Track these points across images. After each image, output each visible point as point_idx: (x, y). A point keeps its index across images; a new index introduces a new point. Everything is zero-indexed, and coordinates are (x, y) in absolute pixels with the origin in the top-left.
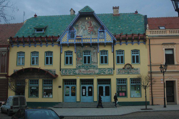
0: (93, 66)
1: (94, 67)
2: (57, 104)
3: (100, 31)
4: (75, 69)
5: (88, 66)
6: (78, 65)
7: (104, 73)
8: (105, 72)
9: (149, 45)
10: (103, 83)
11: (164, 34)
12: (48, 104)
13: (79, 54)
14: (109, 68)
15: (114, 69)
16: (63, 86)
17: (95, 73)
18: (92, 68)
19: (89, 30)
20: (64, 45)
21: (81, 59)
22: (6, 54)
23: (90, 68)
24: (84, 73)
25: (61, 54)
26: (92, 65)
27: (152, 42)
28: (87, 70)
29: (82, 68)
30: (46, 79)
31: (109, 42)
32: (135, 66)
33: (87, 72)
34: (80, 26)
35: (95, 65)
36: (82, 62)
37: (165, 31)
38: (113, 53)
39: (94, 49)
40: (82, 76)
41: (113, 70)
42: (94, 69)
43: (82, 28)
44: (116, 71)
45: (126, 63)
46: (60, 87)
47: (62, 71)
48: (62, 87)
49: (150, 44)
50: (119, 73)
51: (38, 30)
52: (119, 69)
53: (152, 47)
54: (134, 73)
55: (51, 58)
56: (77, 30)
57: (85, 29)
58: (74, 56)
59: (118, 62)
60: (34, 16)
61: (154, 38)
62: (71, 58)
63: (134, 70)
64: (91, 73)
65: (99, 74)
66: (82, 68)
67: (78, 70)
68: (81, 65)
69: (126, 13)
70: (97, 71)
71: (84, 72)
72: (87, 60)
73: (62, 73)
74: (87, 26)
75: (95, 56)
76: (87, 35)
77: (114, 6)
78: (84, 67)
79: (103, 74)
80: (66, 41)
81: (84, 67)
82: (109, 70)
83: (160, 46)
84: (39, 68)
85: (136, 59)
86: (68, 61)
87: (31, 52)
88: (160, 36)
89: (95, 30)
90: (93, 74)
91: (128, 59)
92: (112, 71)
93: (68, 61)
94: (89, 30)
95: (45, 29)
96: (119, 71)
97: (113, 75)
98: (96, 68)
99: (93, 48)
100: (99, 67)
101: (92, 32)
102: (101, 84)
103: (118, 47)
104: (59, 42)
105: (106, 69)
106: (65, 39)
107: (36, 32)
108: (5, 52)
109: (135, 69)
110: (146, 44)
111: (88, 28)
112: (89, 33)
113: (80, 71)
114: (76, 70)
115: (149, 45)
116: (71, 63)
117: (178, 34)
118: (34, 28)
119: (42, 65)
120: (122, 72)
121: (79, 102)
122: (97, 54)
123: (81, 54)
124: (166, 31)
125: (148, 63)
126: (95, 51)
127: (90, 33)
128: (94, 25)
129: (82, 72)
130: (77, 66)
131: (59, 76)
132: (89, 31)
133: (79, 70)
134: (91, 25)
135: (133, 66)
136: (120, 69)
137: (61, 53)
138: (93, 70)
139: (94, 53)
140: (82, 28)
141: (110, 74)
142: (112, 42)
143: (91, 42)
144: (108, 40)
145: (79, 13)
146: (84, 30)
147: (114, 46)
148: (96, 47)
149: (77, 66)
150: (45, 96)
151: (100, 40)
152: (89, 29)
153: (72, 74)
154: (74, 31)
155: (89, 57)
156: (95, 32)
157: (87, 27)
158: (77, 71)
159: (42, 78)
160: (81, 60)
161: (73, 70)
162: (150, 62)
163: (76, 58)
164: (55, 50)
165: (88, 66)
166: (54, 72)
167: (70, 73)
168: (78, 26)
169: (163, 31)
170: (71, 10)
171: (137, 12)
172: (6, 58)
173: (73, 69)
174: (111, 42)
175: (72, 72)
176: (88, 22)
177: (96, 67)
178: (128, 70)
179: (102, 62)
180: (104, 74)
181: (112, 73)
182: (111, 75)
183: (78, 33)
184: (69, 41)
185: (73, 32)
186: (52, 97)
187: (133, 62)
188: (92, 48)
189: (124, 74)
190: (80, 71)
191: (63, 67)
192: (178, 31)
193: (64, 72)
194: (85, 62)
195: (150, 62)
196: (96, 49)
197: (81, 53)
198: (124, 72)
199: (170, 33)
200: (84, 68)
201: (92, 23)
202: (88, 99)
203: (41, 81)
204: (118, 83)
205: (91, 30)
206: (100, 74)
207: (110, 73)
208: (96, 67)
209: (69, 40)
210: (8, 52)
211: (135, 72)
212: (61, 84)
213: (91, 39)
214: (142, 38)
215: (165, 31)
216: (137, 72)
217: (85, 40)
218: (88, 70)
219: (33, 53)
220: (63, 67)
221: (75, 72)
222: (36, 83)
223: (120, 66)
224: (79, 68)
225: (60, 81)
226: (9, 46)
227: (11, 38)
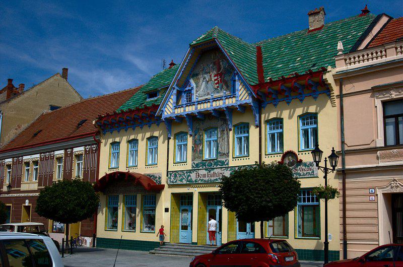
0: (220, 162)
4: (190, 171)
5: (211, 162)
12: (120, 243)
23: (215, 167)
24: (204, 179)
28: (210, 172)
29: (201, 168)
31: (245, 102)
45: (286, 149)
54: (304, 175)
63: (304, 168)
64: (216, 178)
66: (201, 168)
67: (195, 172)
71: (204, 176)
78: (205, 166)
81: (205, 166)
98: (226, 166)
109: (305, 165)
112: (216, 89)
113: (197, 174)
117: (393, 56)
122: (227, 133)
127: (218, 87)
128: (224, 68)
132: (216, 84)
143: (184, 114)
146: (207, 82)
149: (194, 163)
151: (199, 107)
152: (216, 78)
153: (185, 183)
158: (193, 176)
160: (200, 150)
161: (187, 173)
165: (211, 162)
167: (181, 180)
172: (96, 155)
174: (248, 102)
175: (185, 177)
176: (214, 64)
184: (176, 113)
186: (297, 237)
190: (197, 174)
201: (221, 63)
203: (139, 197)
209: (176, 110)
211: (305, 172)
213: (184, 106)
216: (311, 172)
218: (212, 172)
222: (313, 198)
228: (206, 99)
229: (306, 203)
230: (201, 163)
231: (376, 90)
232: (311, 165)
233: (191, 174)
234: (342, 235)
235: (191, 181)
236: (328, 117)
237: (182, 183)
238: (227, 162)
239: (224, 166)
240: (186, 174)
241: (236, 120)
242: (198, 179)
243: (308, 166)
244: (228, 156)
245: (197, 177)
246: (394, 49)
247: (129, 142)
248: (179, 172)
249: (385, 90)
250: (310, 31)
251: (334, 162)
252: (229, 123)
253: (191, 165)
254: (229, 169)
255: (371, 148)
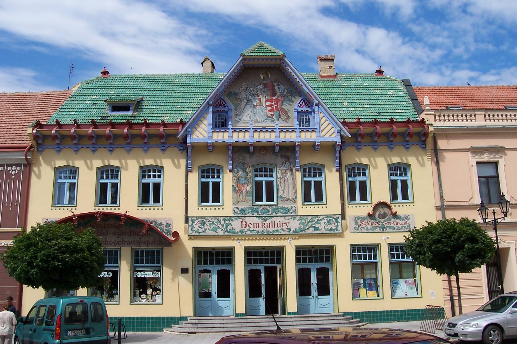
0: (282, 208)
1: (285, 213)
2: (175, 323)
4: (230, 218)
5: (268, 207)
7: (316, 229)
8: (317, 226)
10: (204, 260)
12: (141, 322)
14: (330, 216)
15: (343, 217)
16: (194, 267)
18: (280, 214)
19: (270, 108)
22: (20, 171)
23: (274, 214)
26: (280, 205)
28: (265, 220)
30: (143, 248)
32: (399, 208)
33: (266, 226)
34: (243, 95)
35: (288, 205)
39: (283, 161)
45: (375, 201)
47: (192, 224)
48: (190, 271)
50: (356, 229)
51: (116, 108)
52: (356, 219)
54: (398, 228)
55: (157, 187)
58: (227, 181)
59: (353, 198)
64: (276, 228)
65: (299, 234)
66: (250, 215)
67: (240, 220)
70: (295, 224)
71: (256, 225)
72: (263, 193)
78: (257, 212)
80: (206, 135)
81: (257, 212)
82: (329, 222)
84: (124, 215)
85: (400, 189)
86: (210, 194)
90: (282, 232)
91: (379, 188)
92: (337, 222)
93: (210, 194)
94: (270, 108)
95: (138, 105)
96: (356, 222)
97: (340, 235)
98: (293, 214)
99: (282, 156)
101: (276, 114)
105: (321, 217)
106: (203, 133)
108: (17, 165)
110: (427, 148)
112: (269, 117)
113: (244, 223)
114: (232, 219)
116: (217, 199)
119: (128, 204)
120: (364, 226)
122: (292, 175)
125: (434, 201)
127: (272, 115)
129: (250, 225)
130: (236, 210)
131: (184, 237)
132: (269, 111)
133: (242, 222)
135: (395, 208)
136: (360, 217)
138: (282, 220)
141: (332, 232)
142: (338, 139)
147: (342, 151)
148: (289, 154)
149: (237, 208)
150: (138, 299)
152: (269, 103)
154: (226, 109)
155: (270, 185)
158: (236, 225)
159: (130, 243)
161: (224, 220)
162: (442, 197)
163: (233, 186)
166: (168, 225)
167: (215, 230)
168: (236, 94)
170: (204, 62)
172: (19, 183)
173: (225, 218)
174: (335, 140)
175: (220, 226)
176: (265, 86)
177: (291, 211)
178: (382, 220)
179: (307, 198)
180: (316, 232)
181: (339, 228)
187: (394, 197)
188: (279, 158)
189: (372, 231)
190: (244, 223)
191: (195, 210)
192: (515, 115)
193: (196, 227)
194: (258, 198)
195: (442, 197)
198: (370, 227)
199: (486, 120)
200: (256, 214)
201: (276, 88)
203: (126, 253)
205: (274, 106)
206: (303, 232)
207: (331, 229)
208: (291, 211)
211: (400, 226)
212: (189, 264)
214: (415, 136)
217: (262, 134)
218: (269, 221)
221: (229, 227)
223: (358, 210)
226: (31, 147)
228: (264, 128)
229: (367, 260)
230: (249, 208)
231: (475, 151)
232: (406, 219)
233: (231, 222)
234: (448, 292)
235: (232, 231)
236: (421, 172)
237: (216, 234)
238: (293, 209)
239: (289, 214)
240: (222, 222)
241: (309, 160)
242: (246, 229)
243: (403, 220)
244: (295, 202)
245: (244, 226)
246: (433, 116)
247: (58, 170)
248: (210, 219)
249: (480, 152)
250: (322, 77)
251: (484, 214)
252: (297, 161)
253: (232, 212)
254: (297, 218)
255: (469, 206)
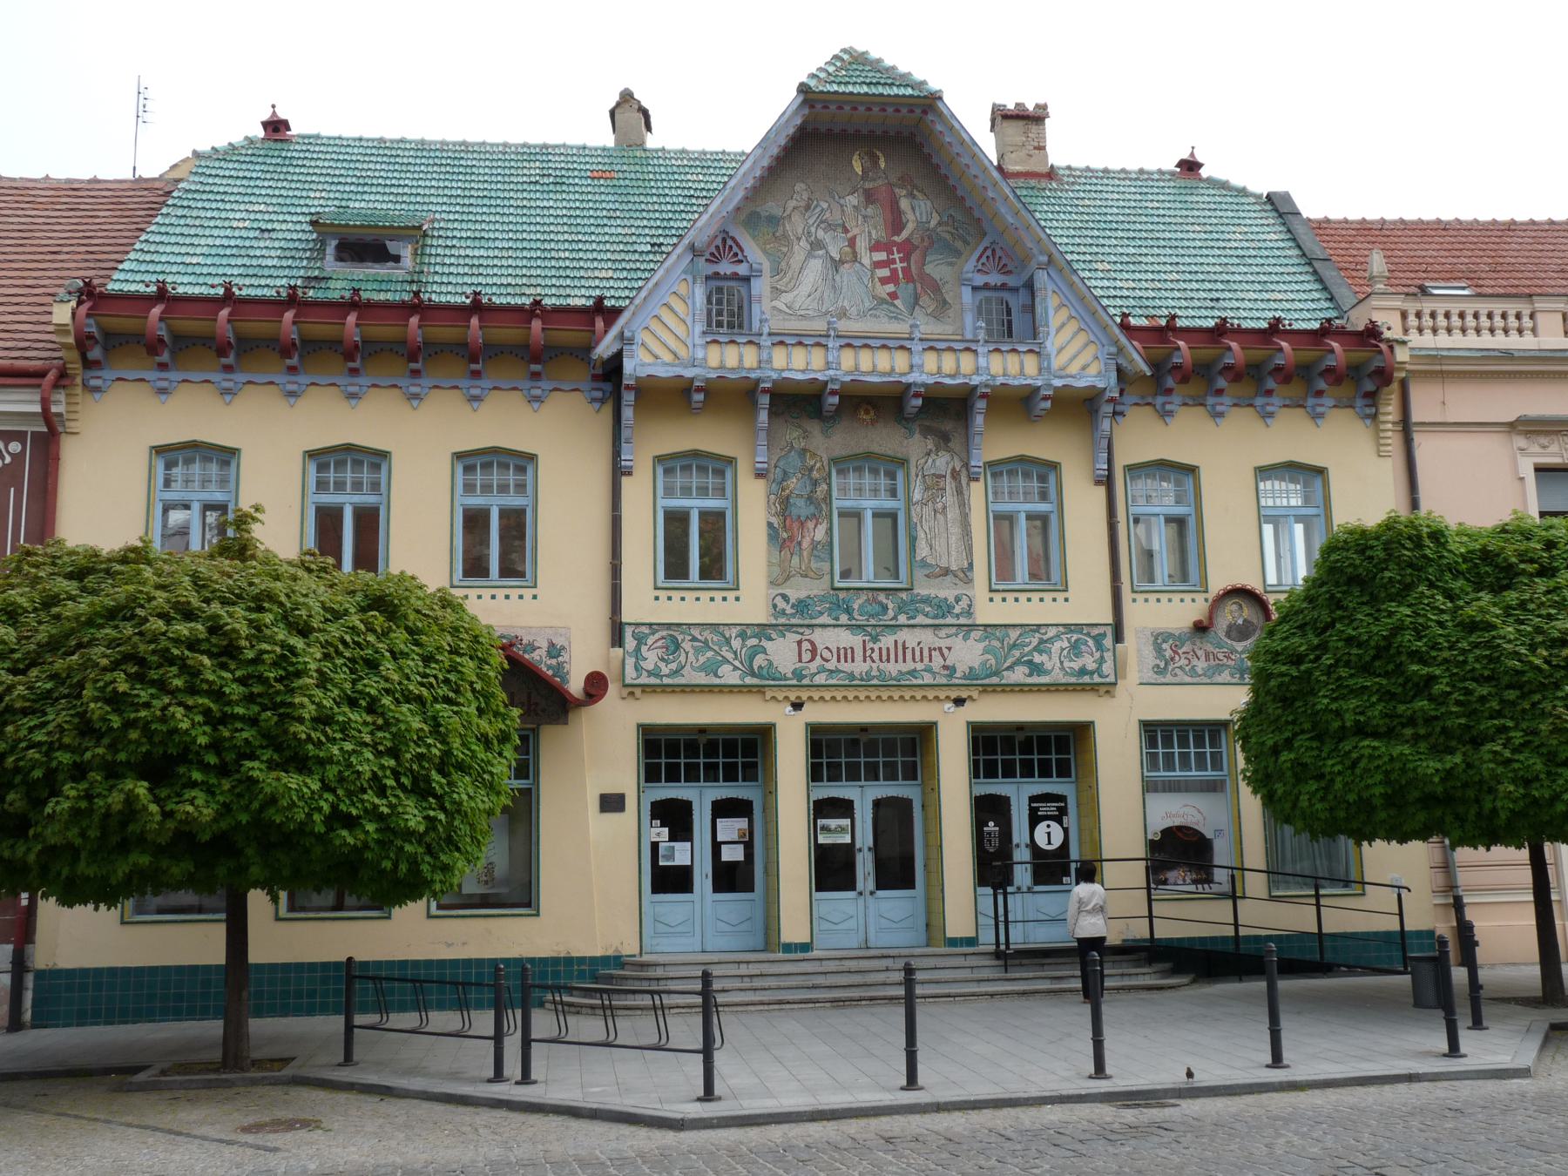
0: (927, 600)
1: (936, 617)
3: (980, 280)
4: (762, 630)
5: (882, 597)
6: (794, 595)
7: (1036, 669)
8: (1037, 659)
9: (1406, 426)
11: (1528, 336)
13: (793, 483)
14: (1078, 627)
15: (1118, 637)
17: (951, 670)
19: (885, 272)
20: (676, 397)
21: (820, 534)
23: (902, 619)
24: (843, 666)
25: (625, 480)
27: (1424, 404)
28: (875, 639)
33: (876, 656)
34: (796, 225)
36: (826, 566)
37: (1526, 312)
38: (1102, 490)
40: (931, 694)
41: (1108, 642)
42: (943, 633)
43: (817, 245)
44: (1136, 651)
45: (1217, 584)
46: (612, 803)
49: (1416, 416)
53: (1425, 447)
56: (766, 266)
57: (842, 262)
60: (260, 133)
61: (1442, 369)
62: (715, 524)
64: (910, 665)
65: (987, 684)
67: (792, 637)
68: (816, 588)
69: (1106, 171)
70: (968, 654)
71: (846, 654)
73: (637, 668)
74: (867, 230)
75: (945, 508)
76: (862, 315)
77: (999, 102)
78: (849, 611)
79: (1030, 680)
81: (849, 611)
82: (1075, 649)
83: (1493, 447)
86: (695, 551)
87: (311, 454)
88: (1488, 356)
89: (937, 269)
90: (928, 679)
93: (695, 551)
94: (885, 272)
96: (1159, 651)
97: (1104, 689)
98: (962, 621)
99: (926, 431)
100: (989, 611)
102: (673, 777)
103: (1140, 438)
104: (612, 369)
105: (1052, 632)
107: (330, 264)
108: (19, 436)
110: (1382, 418)
111: (876, 247)
113: (806, 645)
114: (759, 631)
115: (1406, 426)
116: (714, 567)
118: (313, 223)
120: (1183, 662)
121: (806, 947)
122: (959, 492)
123: (815, 483)
124: (1532, 316)
126: (942, 462)
127: (893, 296)
129: (826, 654)
130: (781, 604)
132: (884, 281)
133: (799, 643)
134: (897, 225)
136: (1171, 635)
137: (618, 472)
138: (927, 638)
139: (934, 485)
140: (817, 245)
144: (1074, 369)
145: (805, 102)
148: (948, 426)
149: (784, 597)
152: (882, 256)
154: (742, 270)
156: (935, 287)
157: (862, 245)
158: (782, 653)
160: (814, 545)
161: (743, 636)
163: (770, 525)
164: (558, 439)
168: (774, 221)
169: (1497, 313)
171: (1199, 165)
173: (745, 630)
175: (730, 656)
177: (957, 610)
181: (1107, 668)
182: (1093, 688)
183: (777, 292)
185: (735, 277)
188: (917, 436)
190: (806, 645)
193: (651, 658)
196: (955, 444)
197: (815, 474)
198: (1201, 665)
200: (844, 619)
201: (904, 204)
202: (872, 917)
204: (1153, 764)
205: (899, 265)
208: (957, 610)
210: (47, 443)
215: (1526, 312)
218: (887, 641)
219: (328, 460)
220: (644, 600)
221: (759, 660)
224: (794, 618)
225: (597, 758)
227: (89, 294)
